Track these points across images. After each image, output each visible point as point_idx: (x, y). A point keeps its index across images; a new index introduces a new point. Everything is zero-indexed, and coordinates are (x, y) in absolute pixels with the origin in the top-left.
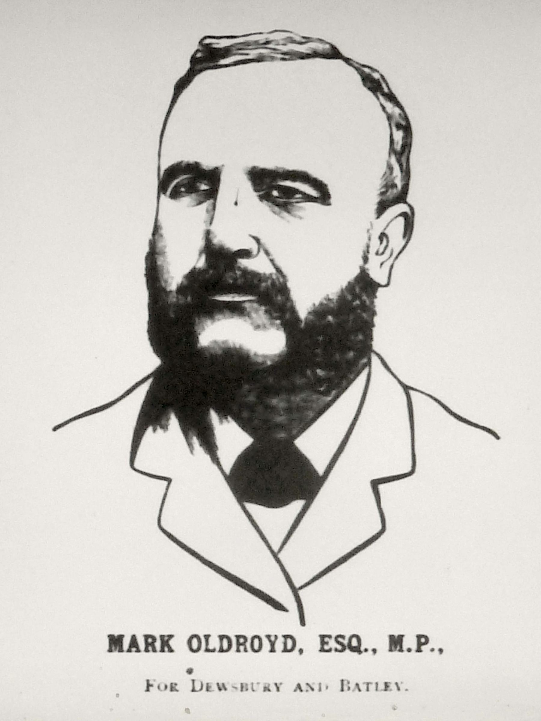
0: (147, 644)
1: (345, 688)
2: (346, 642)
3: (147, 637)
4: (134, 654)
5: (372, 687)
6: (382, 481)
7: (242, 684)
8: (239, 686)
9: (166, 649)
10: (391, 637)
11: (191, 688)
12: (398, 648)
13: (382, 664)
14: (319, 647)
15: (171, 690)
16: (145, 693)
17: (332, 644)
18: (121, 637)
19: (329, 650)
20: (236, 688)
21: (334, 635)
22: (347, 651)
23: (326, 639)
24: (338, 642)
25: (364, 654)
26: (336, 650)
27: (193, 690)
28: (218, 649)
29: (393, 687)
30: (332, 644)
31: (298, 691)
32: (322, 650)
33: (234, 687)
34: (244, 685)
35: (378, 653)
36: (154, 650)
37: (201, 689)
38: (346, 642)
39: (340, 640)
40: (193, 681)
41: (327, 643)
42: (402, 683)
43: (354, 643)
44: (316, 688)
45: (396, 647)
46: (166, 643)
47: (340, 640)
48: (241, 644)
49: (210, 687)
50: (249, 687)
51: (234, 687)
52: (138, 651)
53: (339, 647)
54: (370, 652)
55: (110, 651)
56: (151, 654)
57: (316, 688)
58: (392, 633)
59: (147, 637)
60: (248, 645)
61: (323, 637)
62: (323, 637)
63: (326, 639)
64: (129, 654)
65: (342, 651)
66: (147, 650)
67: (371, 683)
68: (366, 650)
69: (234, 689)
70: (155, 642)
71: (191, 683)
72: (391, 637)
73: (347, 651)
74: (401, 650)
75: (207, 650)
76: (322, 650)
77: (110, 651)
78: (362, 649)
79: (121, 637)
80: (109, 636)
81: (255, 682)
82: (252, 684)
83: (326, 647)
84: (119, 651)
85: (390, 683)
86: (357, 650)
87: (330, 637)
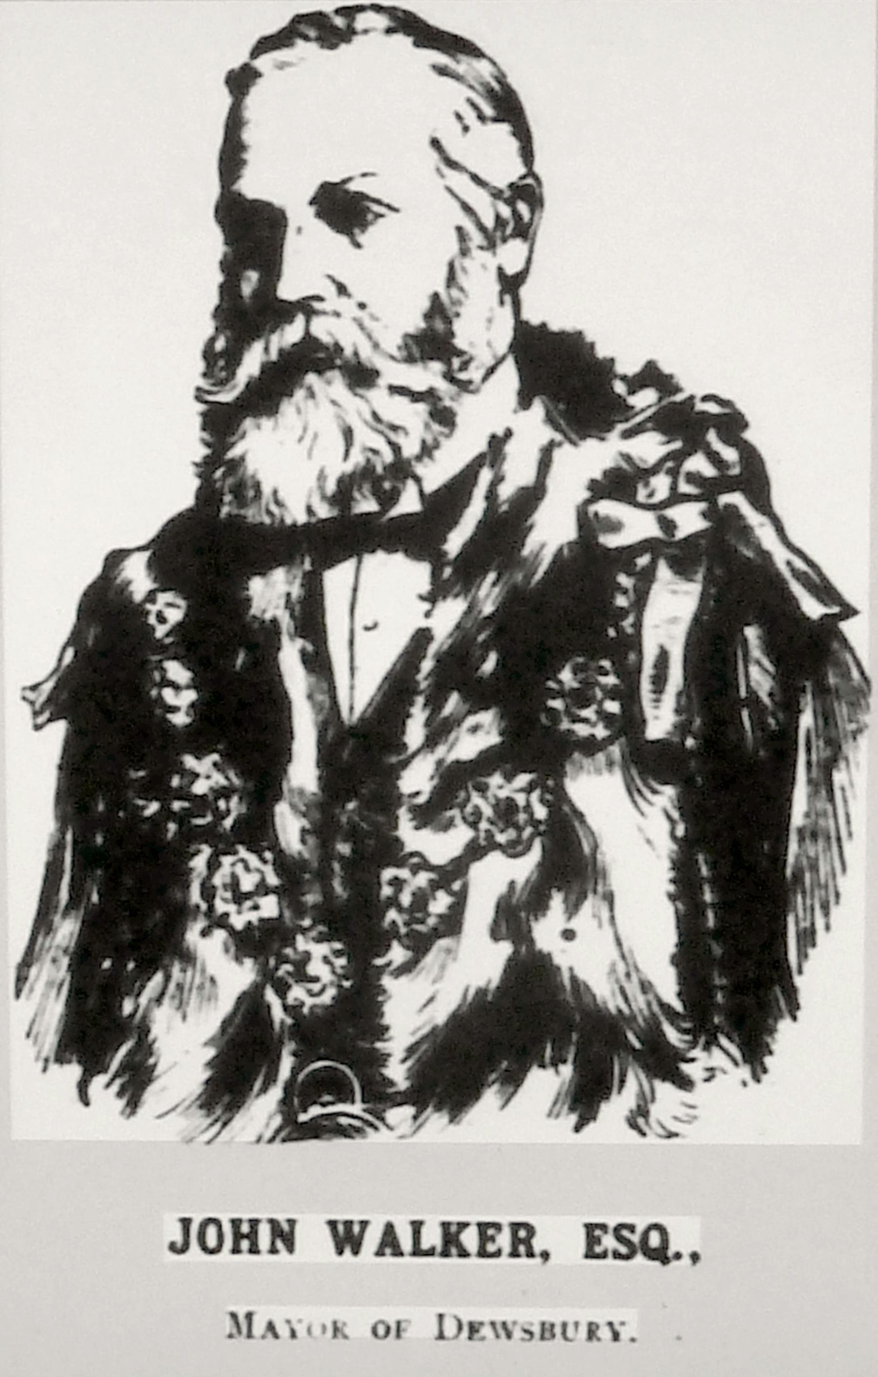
1: (547, 1335)
2: (635, 1238)
7: (543, 1324)
8: (536, 1330)
9: (454, 1251)
11: (435, 1332)
14: (582, 1248)
16: (434, 1341)
17: (609, 1242)
19: (604, 1255)
20: (531, 1333)
21: (612, 1223)
22: (639, 1259)
23: (598, 1232)
24: (620, 1239)
25: (674, 1264)
26: (617, 1255)
27: (441, 1336)
28: (439, 1249)
29: (605, 1333)
30: (609, 1242)
31: (270, 1335)
32: (590, 1254)
33: (526, 1331)
34: (547, 1326)
35: (699, 1265)
36: (254, 1250)
37: (456, 1337)
38: (635, 1238)
39: (625, 1233)
40: (441, 1317)
41: (598, 1241)
42: (623, 1324)
43: (655, 1240)
46: (284, 1236)
47: (625, 1233)
48: (244, 1236)
49: (405, 1330)
50: (558, 1330)
51: (526, 1331)
52: (398, 1253)
53: (623, 1250)
54: (686, 1261)
61: (590, 1228)
62: (590, 1228)
63: (491, 1232)
65: (627, 1257)
68: (678, 1256)
69: (527, 1336)
71: (435, 1321)
73: (639, 1259)
74: (530, 1254)
75: (417, 1252)
76: (590, 1254)
78: (670, 1253)
81: (570, 1322)
82: (564, 1325)
83: (598, 1249)
85: (406, 1321)
86: (661, 1255)
87: (603, 1227)
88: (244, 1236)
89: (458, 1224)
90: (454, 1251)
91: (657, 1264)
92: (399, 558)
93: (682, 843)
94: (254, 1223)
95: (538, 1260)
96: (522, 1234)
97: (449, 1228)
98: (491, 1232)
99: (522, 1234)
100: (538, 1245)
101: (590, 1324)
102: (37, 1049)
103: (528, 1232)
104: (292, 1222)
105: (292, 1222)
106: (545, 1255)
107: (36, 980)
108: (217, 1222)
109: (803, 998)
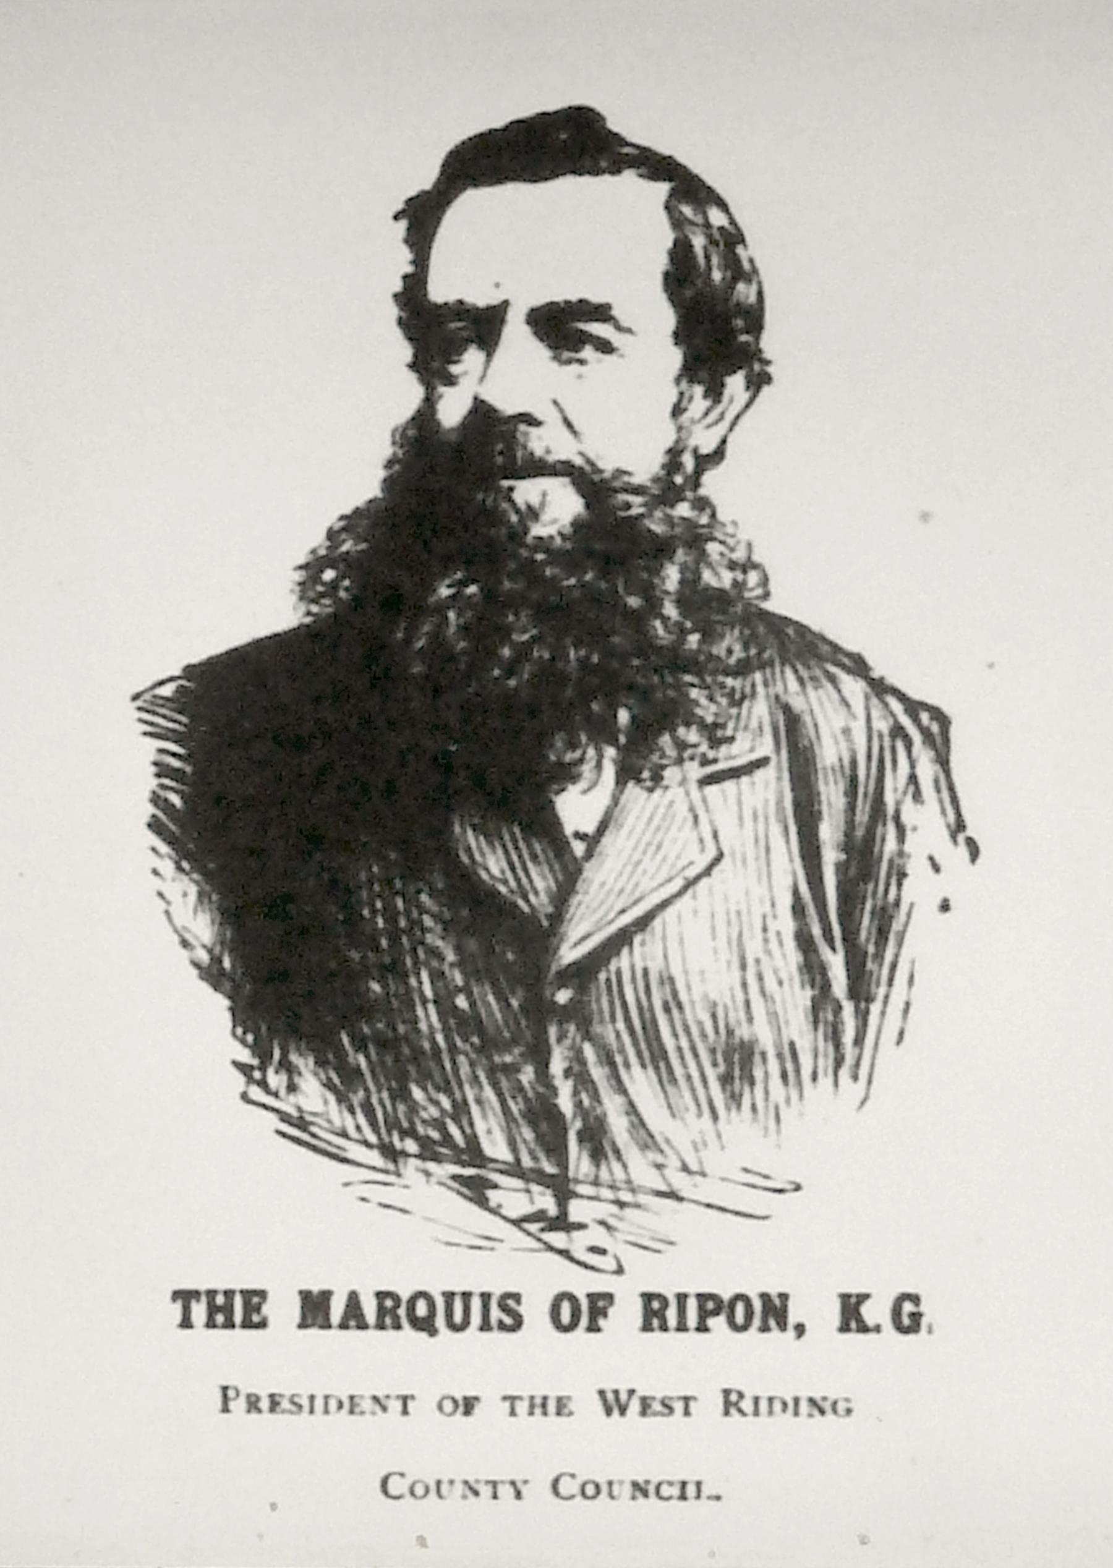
0: (381, 1311)
3: (381, 1296)
4: (353, 1334)
5: (777, 1406)
6: (827, 929)
9: (853, 1325)
10: (306, 1296)
12: (320, 1320)
13: (819, 1358)
15: (352, 1412)
18: (326, 1295)
20: (300, 1407)
36: (664, 1328)
44: (804, 1407)
45: (314, 1319)
48: (219, 1309)
52: (363, 1326)
55: (303, 1325)
56: (657, 1335)
57: (804, 1407)
58: (304, 1287)
59: (381, 1296)
60: (402, 1312)
63: (256, 1300)
64: (344, 1332)
66: (381, 1326)
67: (520, 1398)
70: (399, 1307)
72: (306, 1296)
77: (303, 1325)
79: (326, 1295)
80: (301, 1292)
84: (322, 1327)
88: (219, 1309)
89: (858, 1296)
90: (853, 1325)
91: (423, 1335)
92: (428, 185)
93: (654, 747)
94: (229, 1294)
95: (791, 1333)
96: (656, 1305)
97: (214, 1299)
98: (601, 1304)
99: (656, 1305)
100: (792, 1319)
101: (272, 1396)
102: (771, 1098)
103: (393, 1299)
104: (784, 1297)
105: (784, 1297)
106: (800, 1329)
107: (786, 1012)
108: (572, 1298)
109: (205, 989)
